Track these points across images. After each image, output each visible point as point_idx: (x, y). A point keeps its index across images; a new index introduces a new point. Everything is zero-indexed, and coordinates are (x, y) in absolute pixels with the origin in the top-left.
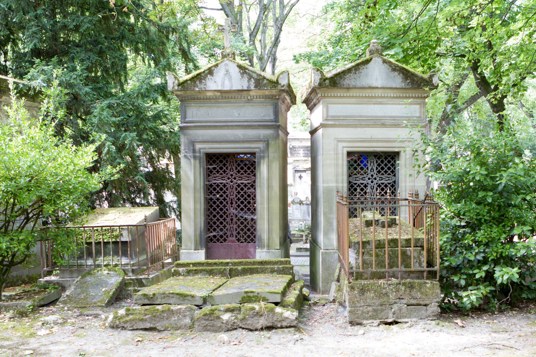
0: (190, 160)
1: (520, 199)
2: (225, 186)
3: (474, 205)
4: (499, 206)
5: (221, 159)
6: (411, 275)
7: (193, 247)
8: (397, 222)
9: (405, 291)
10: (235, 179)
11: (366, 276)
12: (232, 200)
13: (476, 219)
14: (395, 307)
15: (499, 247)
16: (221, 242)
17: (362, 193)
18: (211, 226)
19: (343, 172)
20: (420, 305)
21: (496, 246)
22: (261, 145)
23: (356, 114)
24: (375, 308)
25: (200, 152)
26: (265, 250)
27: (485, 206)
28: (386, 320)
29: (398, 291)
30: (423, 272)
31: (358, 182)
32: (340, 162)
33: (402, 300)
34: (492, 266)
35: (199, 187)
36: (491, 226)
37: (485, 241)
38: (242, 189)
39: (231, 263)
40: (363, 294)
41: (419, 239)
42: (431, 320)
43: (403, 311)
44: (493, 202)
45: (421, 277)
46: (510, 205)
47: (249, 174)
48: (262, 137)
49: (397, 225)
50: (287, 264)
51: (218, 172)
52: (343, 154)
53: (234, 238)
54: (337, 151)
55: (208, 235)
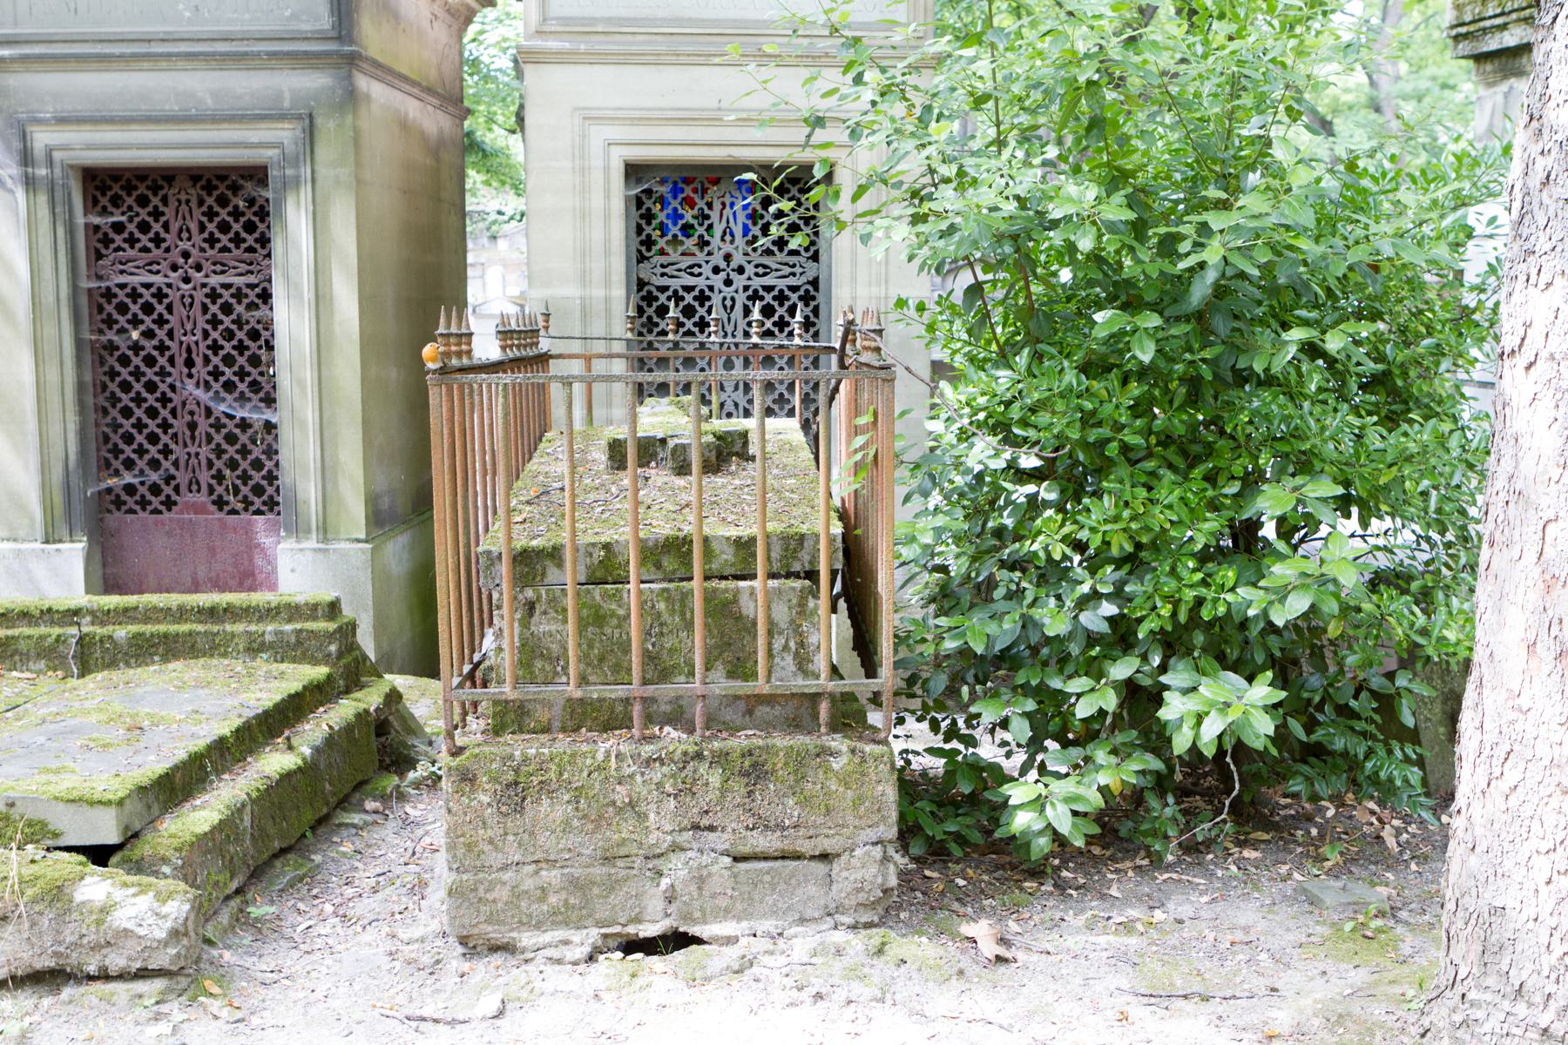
0: (11, 191)
1: (1292, 350)
2: (160, 295)
3: (1070, 377)
4: (1194, 384)
5: (142, 190)
6: (762, 711)
7: (39, 532)
8: (753, 449)
9: (724, 791)
10: (199, 268)
11: (542, 715)
12: (189, 350)
13: (1084, 444)
14: (677, 870)
15: (1185, 574)
16: (156, 512)
17: (689, 324)
18: (116, 451)
19: (607, 241)
20: (798, 857)
21: (1173, 571)
22: (286, 134)
23: (661, 14)
24: (577, 872)
25: (50, 163)
26: (312, 543)
27: (1125, 382)
28: (631, 929)
29: (687, 790)
30: (815, 698)
31: (675, 284)
32: (597, 202)
33: (711, 836)
34: (1156, 661)
35: (51, 299)
36: (1153, 474)
37: (1121, 545)
38: (227, 309)
39: (92, 612)
40: (519, 809)
41: (802, 538)
42: (854, 927)
43: (715, 884)
44: (1162, 364)
45: (807, 720)
46: (1242, 378)
47: (251, 250)
48: (286, 104)
49: (753, 458)
50: (315, 619)
51: (132, 241)
52: (607, 169)
53: (202, 498)
54: (582, 157)
55: (103, 486)
